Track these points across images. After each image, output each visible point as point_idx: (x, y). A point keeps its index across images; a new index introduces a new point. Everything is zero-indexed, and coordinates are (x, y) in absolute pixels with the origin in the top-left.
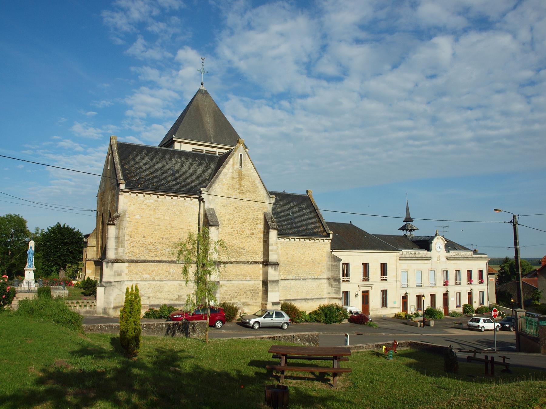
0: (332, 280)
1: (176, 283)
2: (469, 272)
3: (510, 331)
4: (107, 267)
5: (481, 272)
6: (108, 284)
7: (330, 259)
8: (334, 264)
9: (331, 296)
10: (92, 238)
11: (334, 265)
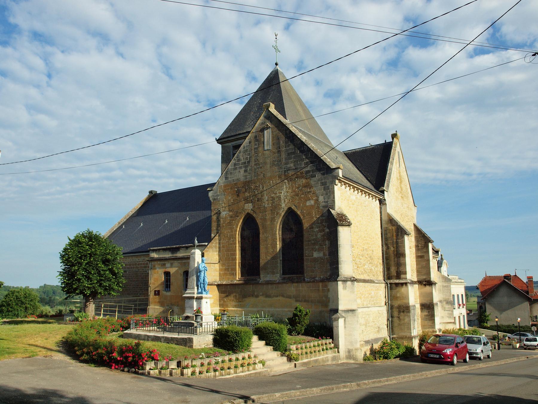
0: (444, 303)
1: (376, 309)
2: (458, 295)
3: (452, 363)
4: (345, 288)
5: (462, 295)
6: (350, 313)
7: (441, 279)
8: (445, 284)
9: (445, 321)
10: (211, 250)
11: (445, 286)
